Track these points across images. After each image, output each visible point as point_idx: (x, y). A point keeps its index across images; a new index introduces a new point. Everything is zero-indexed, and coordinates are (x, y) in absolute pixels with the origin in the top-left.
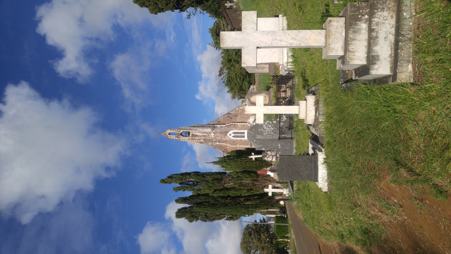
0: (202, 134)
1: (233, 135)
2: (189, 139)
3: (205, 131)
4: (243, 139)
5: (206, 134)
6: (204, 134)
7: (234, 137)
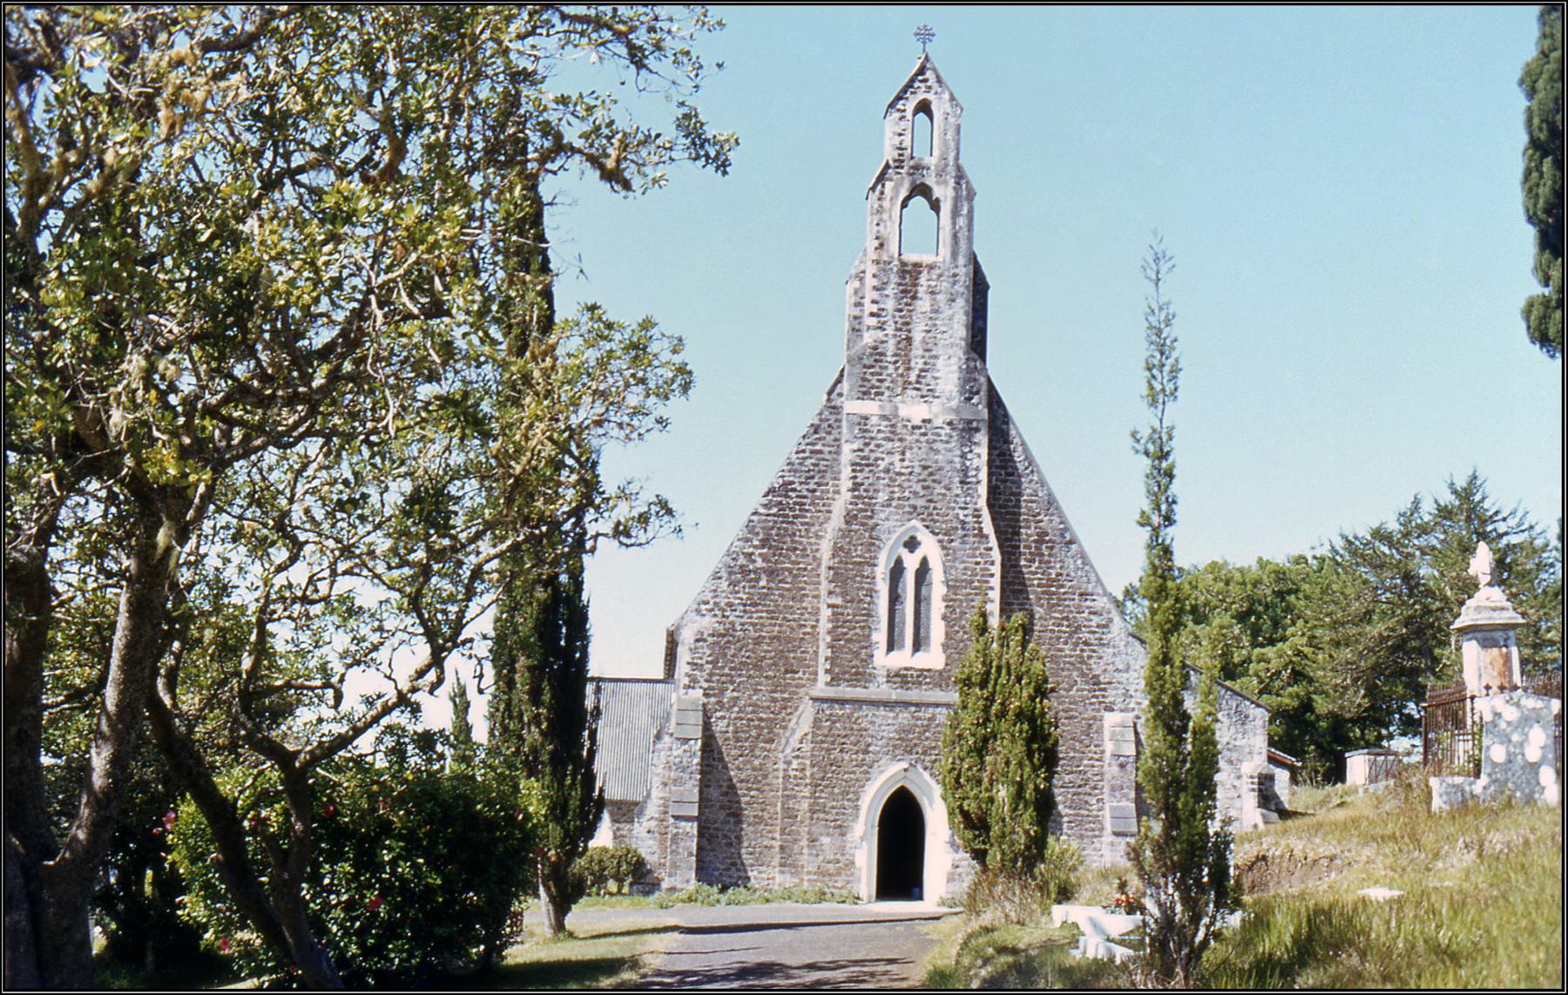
0: (918, 336)
1: (911, 562)
2: (881, 245)
3: (940, 363)
4: (880, 636)
5: (918, 364)
6: (917, 350)
7: (897, 571)
